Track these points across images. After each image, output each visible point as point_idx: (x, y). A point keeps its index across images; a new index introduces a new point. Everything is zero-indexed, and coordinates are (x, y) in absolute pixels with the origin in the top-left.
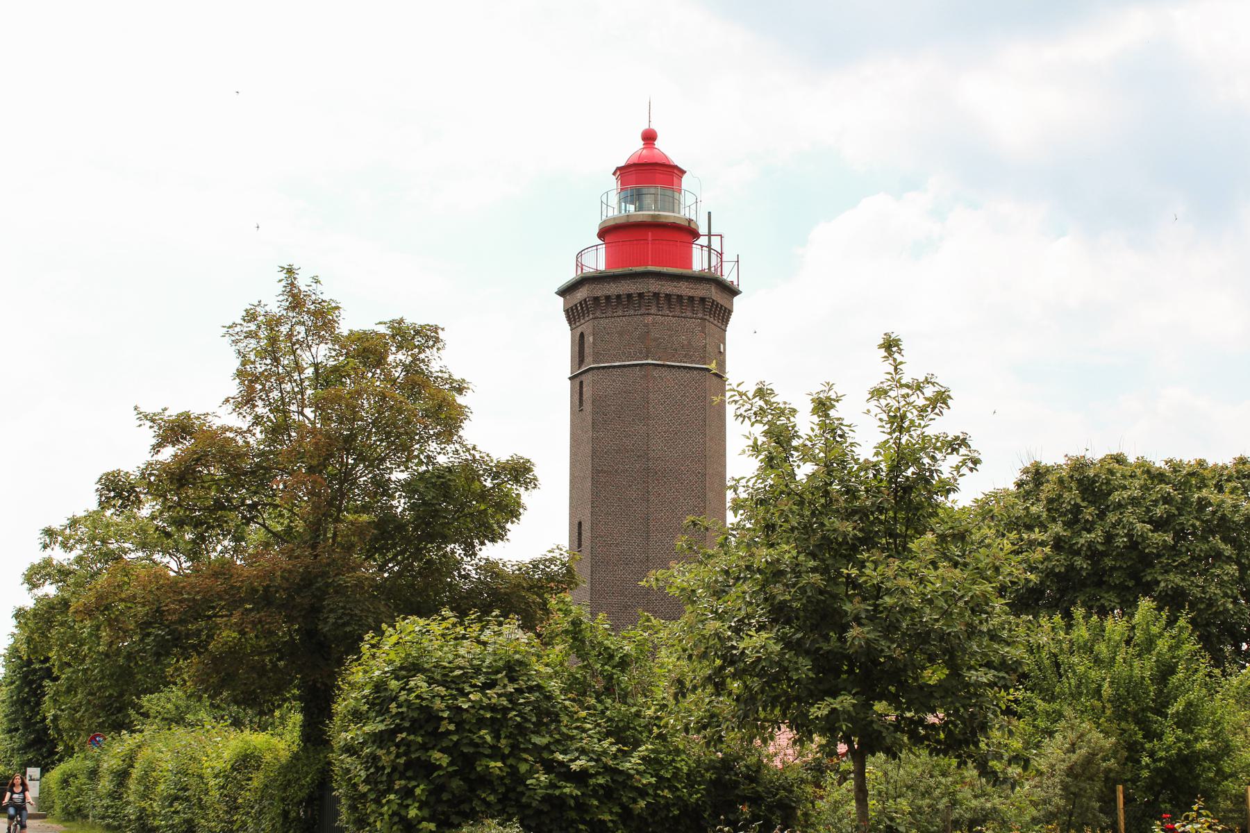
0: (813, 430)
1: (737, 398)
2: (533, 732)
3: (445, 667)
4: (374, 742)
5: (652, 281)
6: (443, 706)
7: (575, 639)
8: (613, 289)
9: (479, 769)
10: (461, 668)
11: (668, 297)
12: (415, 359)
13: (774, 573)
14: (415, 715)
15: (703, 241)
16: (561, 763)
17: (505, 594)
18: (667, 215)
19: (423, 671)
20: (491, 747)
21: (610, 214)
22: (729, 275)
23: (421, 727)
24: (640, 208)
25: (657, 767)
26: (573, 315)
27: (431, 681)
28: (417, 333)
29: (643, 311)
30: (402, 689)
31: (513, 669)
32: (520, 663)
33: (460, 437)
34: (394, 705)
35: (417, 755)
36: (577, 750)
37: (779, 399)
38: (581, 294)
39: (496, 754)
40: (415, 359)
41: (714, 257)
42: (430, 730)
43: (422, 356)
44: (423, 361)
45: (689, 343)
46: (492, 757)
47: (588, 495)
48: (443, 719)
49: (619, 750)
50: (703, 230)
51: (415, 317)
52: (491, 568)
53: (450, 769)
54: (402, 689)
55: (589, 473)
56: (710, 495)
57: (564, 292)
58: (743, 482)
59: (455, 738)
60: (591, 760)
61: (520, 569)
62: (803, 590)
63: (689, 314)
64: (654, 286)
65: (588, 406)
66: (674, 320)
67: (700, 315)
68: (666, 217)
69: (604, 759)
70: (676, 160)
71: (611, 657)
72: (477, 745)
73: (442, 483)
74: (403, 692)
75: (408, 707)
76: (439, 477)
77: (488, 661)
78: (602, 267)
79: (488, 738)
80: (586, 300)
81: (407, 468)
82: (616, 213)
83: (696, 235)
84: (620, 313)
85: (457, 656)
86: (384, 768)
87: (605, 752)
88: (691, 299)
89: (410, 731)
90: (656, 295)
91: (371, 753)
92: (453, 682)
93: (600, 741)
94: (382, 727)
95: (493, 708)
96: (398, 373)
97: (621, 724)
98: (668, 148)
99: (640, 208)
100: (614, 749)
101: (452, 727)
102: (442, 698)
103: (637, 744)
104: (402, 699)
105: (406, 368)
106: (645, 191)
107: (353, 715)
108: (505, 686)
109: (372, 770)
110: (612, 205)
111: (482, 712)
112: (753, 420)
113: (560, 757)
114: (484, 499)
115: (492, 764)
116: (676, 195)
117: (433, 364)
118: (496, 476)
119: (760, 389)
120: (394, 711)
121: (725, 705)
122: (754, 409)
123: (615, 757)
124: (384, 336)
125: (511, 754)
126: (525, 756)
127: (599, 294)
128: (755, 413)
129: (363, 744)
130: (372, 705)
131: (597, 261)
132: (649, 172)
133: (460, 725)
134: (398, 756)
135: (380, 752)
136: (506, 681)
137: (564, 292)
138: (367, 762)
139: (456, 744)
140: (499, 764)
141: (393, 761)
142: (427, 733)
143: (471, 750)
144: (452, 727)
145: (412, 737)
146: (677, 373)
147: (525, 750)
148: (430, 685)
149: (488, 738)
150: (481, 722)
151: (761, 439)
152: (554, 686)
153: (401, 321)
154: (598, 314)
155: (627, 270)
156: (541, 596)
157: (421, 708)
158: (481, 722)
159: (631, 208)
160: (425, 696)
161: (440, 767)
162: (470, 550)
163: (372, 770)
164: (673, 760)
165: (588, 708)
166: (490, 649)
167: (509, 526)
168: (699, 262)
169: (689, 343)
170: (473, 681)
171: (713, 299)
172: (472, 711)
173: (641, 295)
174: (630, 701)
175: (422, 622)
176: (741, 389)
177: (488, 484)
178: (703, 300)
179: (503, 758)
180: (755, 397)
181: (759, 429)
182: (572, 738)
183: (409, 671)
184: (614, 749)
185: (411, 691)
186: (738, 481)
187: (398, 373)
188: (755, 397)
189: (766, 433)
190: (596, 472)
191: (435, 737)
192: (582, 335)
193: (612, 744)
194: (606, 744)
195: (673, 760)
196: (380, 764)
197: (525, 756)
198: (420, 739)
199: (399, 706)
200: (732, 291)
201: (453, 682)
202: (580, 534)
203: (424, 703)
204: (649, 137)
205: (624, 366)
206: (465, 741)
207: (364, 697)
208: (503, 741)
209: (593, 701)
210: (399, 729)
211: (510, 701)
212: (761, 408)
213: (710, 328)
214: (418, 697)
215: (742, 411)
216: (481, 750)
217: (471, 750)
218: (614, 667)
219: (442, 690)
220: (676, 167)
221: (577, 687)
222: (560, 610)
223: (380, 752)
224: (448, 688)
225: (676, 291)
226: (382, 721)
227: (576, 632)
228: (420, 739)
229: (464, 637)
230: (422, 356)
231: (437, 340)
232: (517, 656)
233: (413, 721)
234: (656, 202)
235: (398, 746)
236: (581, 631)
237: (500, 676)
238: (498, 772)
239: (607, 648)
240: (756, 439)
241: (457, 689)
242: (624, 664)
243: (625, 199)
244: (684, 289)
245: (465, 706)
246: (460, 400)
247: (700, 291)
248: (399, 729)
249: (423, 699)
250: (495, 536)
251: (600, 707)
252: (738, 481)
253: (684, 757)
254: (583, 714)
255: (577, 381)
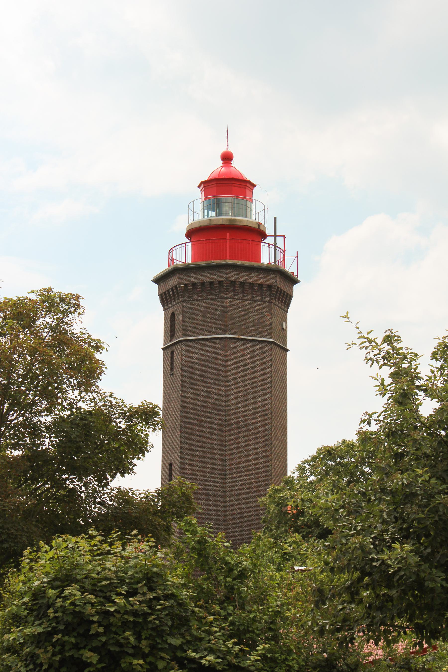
0: (432, 372)
1: (367, 344)
2: (168, 635)
3: (93, 578)
4: (32, 643)
5: (229, 271)
6: (93, 611)
7: (200, 555)
8: (199, 278)
9: (123, 665)
10: (106, 579)
11: (242, 284)
12: (60, 322)
13: (407, 496)
14: (70, 619)
15: (270, 240)
16: (193, 660)
17: (136, 518)
18: (242, 220)
19: (77, 581)
20: (134, 647)
21: (196, 219)
22: (290, 267)
23: (74, 630)
24: (219, 214)
25: (272, 665)
26: (165, 299)
27: (83, 590)
28: (62, 300)
29: (222, 295)
30: (59, 597)
31: (151, 579)
32: (158, 575)
33: (97, 387)
34: (51, 610)
35: (71, 654)
36: (206, 649)
37: (402, 345)
38: (173, 282)
39: (138, 653)
40: (60, 322)
41: (278, 253)
42: (81, 632)
43: (66, 320)
44: (67, 324)
45: (259, 320)
46: (134, 656)
47: (177, 440)
48: (94, 622)
49: (241, 650)
50: (269, 231)
51: (61, 288)
52: (123, 496)
53: (99, 666)
54: (59, 597)
55: (178, 423)
56: (275, 442)
57: (158, 280)
58: (375, 416)
59: (104, 639)
60: (219, 657)
61: (147, 497)
62: (435, 510)
63: (259, 298)
64: (231, 276)
65: (178, 372)
66: (246, 303)
67: (268, 299)
68: (241, 221)
69: (229, 658)
70: (248, 176)
71: (231, 570)
72: (121, 645)
73: (85, 425)
74: (59, 600)
75: (63, 612)
76: (81, 419)
77: (130, 573)
78: (189, 260)
79: (132, 639)
80: (175, 286)
81: (51, 413)
82: (201, 217)
83: (264, 235)
84: (204, 297)
85: (104, 569)
86: (41, 665)
87: (229, 651)
88: (261, 286)
89: (66, 632)
90: (233, 283)
91: (29, 653)
92: (100, 591)
93: (224, 642)
94: (40, 630)
95: (135, 614)
96: (46, 335)
97: (242, 628)
98: (242, 166)
99: (219, 214)
100: (237, 649)
101: (101, 630)
102: (93, 605)
103: (253, 646)
104: (58, 605)
105: (52, 329)
106: (223, 200)
107: (13, 619)
108: (144, 594)
109: (31, 667)
110: (198, 212)
111: (126, 616)
112: (381, 363)
113: (193, 654)
114: (103, 441)
115: (135, 662)
116: (249, 203)
117: (75, 326)
118: (130, 418)
119: (388, 336)
120: (52, 615)
121: (357, 611)
122: (382, 354)
123: (237, 656)
124: (35, 302)
125: (150, 654)
126: (163, 655)
127: (187, 281)
128: (383, 357)
129: (22, 645)
130: (31, 610)
131: (185, 256)
132: (227, 186)
133: (107, 628)
134: (54, 655)
135: (37, 651)
136: (145, 589)
137: (158, 280)
138: (26, 660)
139: (105, 644)
140: (141, 662)
141: (50, 659)
142: (79, 635)
143: (117, 649)
144: (101, 630)
145: (66, 638)
146: (249, 345)
147: (161, 650)
148: (83, 593)
149: (132, 639)
150: (125, 625)
151: (388, 381)
152: (185, 594)
153: (50, 290)
154: (186, 298)
155: (203, 263)
156: (164, 519)
157: (74, 613)
158: (125, 625)
159: (213, 214)
160: (78, 603)
161: (90, 664)
162: (102, 481)
163: (31, 667)
164: (286, 659)
165: (214, 615)
166: (132, 563)
167: (135, 461)
168: (266, 257)
169: (259, 320)
170: (119, 590)
171: (278, 286)
172: (118, 616)
173: (220, 283)
174: (248, 608)
175: (74, 539)
176: (371, 336)
177: (123, 425)
178: (270, 287)
179: (144, 656)
180: (383, 343)
181: (387, 371)
182: (201, 640)
183: (63, 581)
184: (237, 649)
185: (65, 598)
186: (371, 415)
187: (46, 335)
188: (383, 343)
189: (392, 375)
190: (184, 424)
191: (87, 636)
192: (173, 314)
193: (235, 644)
194: (230, 644)
195: (286, 659)
196: (38, 662)
197: (163, 655)
198: (73, 640)
199: (56, 612)
200: (292, 280)
201: (100, 591)
202: (170, 473)
203: (77, 609)
204: (227, 158)
205: (207, 339)
206: (111, 642)
207: (25, 604)
208: (144, 642)
209: (218, 608)
210: (55, 631)
211: (150, 607)
212: (388, 353)
213: (276, 310)
214: (72, 604)
215: (371, 355)
216: (126, 649)
217: (117, 649)
218: (234, 579)
219: (91, 597)
220: (248, 182)
221: (203, 597)
222: (188, 531)
223: (37, 651)
224: (97, 596)
225: (249, 280)
226: (40, 625)
227: (201, 549)
228: (73, 640)
229: (109, 553)
230: (66, 320)
231: (78, 306)
232: (155, 569)
233: (67, 624)
234: (232, 209)
235: (54, 646)
236: (205, 548)
237: (140, 585)
238: (139, 668)
239: (227, 563)
240: (383, 380)
241: (105, 597)
242: (242, 576)
243: (208, 208)
244: (255, 278)
245: (112, 609)
246: (97, 356)
247: (267, 280)
248: (55, 631)
249: (76, 606)
250: (125, 470)
251: (223, 613)
252: (371, 415)
253: (295, 656)
254: (211, 618)
255: (169, 351)
